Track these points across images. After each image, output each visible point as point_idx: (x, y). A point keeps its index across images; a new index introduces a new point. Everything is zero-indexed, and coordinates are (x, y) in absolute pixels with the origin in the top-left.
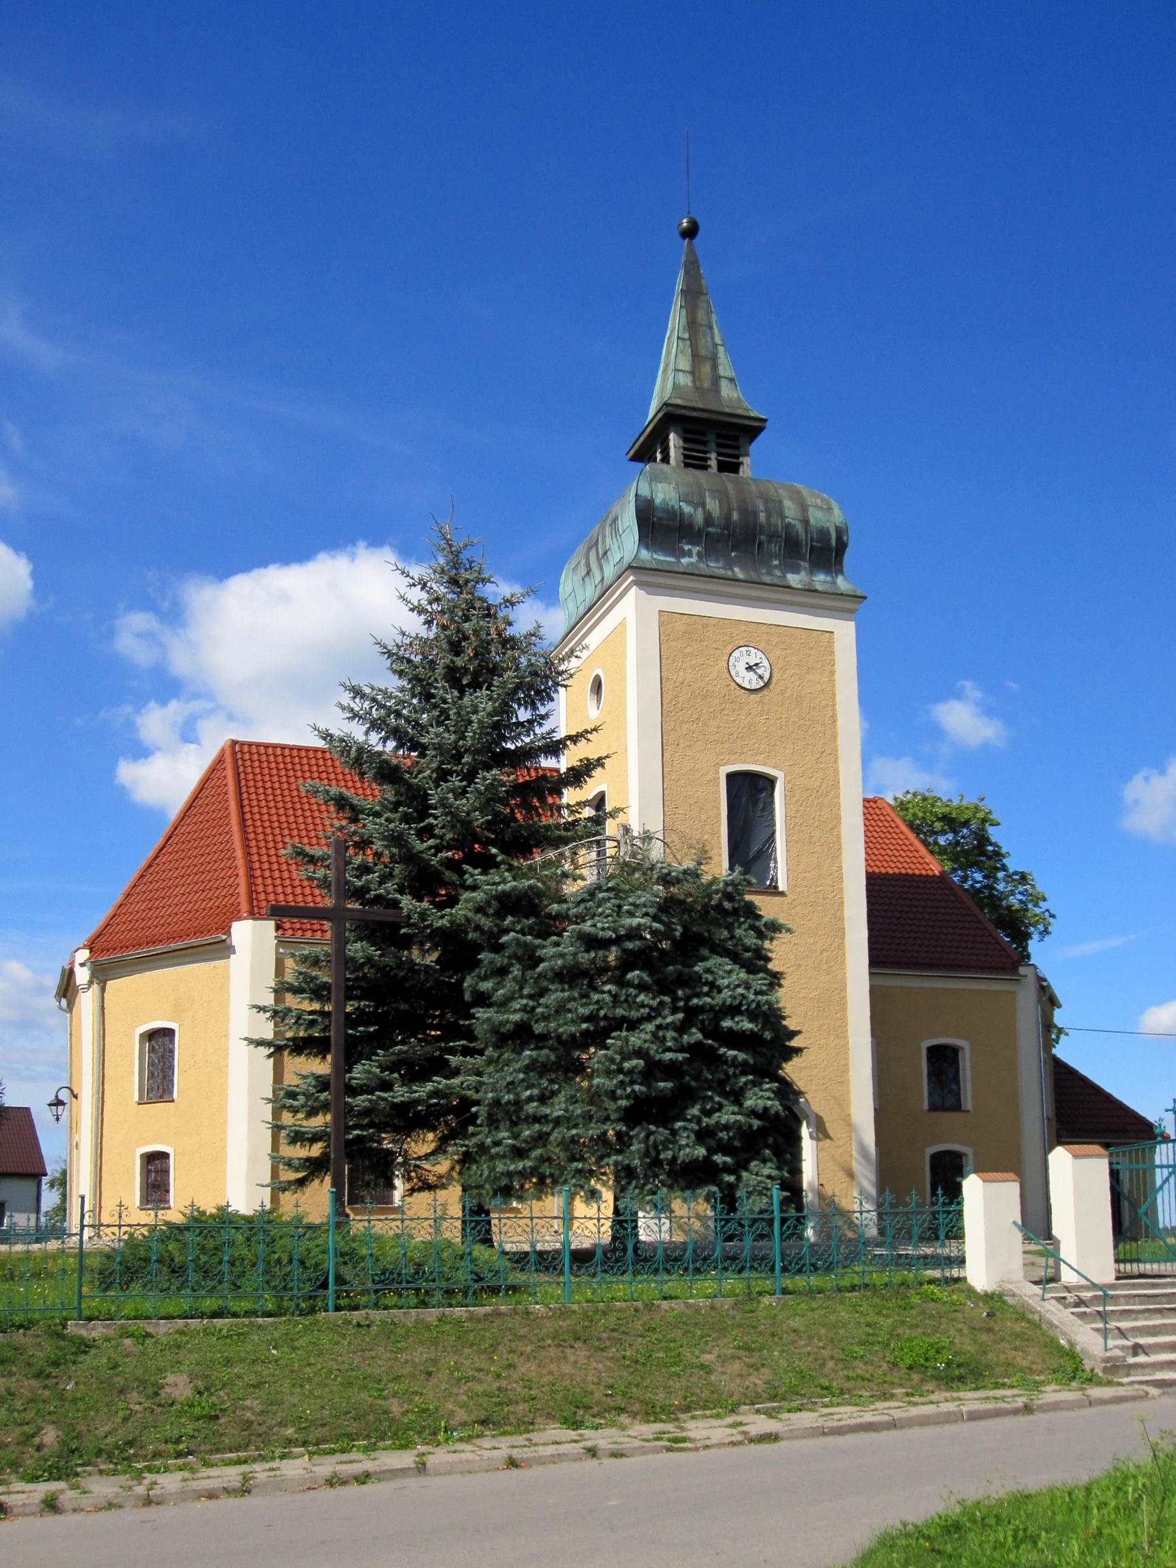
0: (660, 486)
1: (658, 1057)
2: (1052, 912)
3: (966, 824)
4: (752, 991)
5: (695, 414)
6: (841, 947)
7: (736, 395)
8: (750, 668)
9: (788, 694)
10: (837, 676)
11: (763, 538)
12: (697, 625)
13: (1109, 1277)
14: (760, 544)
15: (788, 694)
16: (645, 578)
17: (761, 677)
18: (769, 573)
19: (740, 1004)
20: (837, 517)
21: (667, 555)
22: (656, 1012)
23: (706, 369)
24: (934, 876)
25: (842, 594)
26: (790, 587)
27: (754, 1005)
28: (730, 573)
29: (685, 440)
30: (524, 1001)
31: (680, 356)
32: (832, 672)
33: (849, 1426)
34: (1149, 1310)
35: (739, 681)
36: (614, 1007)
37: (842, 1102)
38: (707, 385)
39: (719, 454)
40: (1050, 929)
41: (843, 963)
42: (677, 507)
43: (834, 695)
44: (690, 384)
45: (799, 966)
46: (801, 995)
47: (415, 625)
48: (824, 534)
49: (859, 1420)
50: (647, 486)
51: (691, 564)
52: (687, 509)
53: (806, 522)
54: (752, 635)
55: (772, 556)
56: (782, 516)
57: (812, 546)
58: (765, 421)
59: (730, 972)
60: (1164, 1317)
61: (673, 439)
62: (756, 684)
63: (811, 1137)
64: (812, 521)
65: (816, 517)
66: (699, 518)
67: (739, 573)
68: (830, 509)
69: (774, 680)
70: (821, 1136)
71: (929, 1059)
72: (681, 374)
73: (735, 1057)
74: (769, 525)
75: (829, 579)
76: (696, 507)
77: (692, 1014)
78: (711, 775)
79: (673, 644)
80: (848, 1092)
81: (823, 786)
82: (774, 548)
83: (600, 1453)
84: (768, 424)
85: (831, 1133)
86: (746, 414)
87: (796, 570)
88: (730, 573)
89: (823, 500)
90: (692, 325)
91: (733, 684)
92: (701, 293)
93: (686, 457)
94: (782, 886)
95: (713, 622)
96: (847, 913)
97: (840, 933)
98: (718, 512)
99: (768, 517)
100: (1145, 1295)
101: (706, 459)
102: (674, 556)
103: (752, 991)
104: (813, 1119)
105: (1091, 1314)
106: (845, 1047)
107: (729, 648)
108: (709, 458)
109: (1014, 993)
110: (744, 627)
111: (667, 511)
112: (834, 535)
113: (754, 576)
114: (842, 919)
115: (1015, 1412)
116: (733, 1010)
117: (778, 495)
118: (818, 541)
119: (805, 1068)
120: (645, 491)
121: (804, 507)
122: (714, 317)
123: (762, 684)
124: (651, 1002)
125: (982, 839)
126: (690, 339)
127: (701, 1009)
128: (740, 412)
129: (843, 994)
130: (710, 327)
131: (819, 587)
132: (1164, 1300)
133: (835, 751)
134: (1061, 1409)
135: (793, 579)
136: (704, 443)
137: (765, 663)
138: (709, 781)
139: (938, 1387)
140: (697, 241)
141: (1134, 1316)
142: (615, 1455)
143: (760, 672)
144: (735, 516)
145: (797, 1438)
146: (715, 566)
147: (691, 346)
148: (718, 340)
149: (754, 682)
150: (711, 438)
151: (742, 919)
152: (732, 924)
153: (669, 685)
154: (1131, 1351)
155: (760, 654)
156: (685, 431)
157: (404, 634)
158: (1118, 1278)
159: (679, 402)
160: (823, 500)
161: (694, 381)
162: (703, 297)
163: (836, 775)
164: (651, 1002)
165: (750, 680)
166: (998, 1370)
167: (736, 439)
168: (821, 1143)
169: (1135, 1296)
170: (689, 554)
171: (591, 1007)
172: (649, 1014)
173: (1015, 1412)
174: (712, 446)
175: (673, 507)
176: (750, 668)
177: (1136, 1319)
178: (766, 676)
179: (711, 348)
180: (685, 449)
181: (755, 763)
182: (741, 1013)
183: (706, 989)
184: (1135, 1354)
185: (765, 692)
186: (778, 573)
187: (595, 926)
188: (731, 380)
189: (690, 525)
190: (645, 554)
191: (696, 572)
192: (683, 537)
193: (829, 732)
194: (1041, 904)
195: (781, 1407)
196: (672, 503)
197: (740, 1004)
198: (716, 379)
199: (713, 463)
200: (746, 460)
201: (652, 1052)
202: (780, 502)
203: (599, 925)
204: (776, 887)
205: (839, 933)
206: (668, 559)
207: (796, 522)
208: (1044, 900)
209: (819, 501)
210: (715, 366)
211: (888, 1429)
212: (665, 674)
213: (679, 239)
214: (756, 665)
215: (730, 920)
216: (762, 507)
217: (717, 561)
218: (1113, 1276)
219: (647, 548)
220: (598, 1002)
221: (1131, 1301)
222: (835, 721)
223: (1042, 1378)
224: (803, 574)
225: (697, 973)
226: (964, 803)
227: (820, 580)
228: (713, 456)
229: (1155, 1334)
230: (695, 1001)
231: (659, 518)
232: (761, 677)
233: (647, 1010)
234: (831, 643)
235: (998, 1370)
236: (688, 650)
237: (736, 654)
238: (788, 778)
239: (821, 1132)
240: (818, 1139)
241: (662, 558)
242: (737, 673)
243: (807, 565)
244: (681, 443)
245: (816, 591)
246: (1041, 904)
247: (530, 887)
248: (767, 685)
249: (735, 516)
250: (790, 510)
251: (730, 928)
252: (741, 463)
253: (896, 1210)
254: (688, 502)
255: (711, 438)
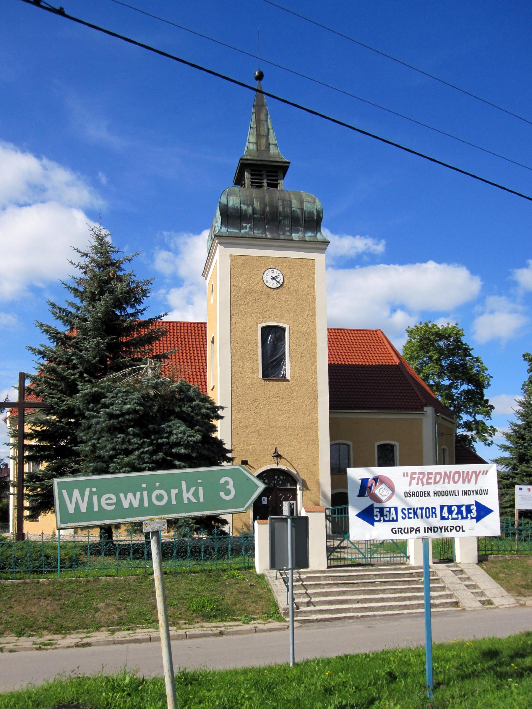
0: (231, 198)
1: (139, 466)
2: (491, 375)
3: (450, 336)
4: (186, 436)
5: (255, 162)
6: (316, 403)
7: (277, 152)
8: (273, 278)
9: (291, 289)
10: (316, 280)
11: (281, 218)
12: (248, 260)
13: (324, 567)
14: (280, 221)
15: (291, 289)
16: (222, 241)
17: (278, 282)
18: (284, 234)
19: (180, 442)
20: (318, 205)
21: (234, 229)
22: (141, 446)
23: (264, 140)
24: (396, 365)
25: (318, 241)
26: (292, 240)
27: (186, 442)
28: (264, 235)
29: (252, 175)
30: (93, 441)
31: (251, 136)
32: (314, 278)
33: (127, 640)
34: (330, 584)
35: (268, 284)
36: (123, 444)
37: (315, 473)
38: (263, 148)
39: (268, 180)
40: (490, 383)
41: (316, 412)
42: (239, 207)
43: (314, 288)
44: (255, 149)
45: (295, 413)
46: (296, 426)
47: (79, 274)
48: (311, 213)
49: (134, 638)
50: (225, 198)
51: (246, 232)
52: (244, 207)
53: (302, 209)
54: (274, 263)
55: (286, 226)
56: (291, 207)
57: (305, 220)
58: (289, 163)
59: (179, 427)
60: (338, 587)
61: (247, 175)
62: (276, 285)
63: (300, 490)
64: (305, 209)
65: (307, 207)
66: (250, 211)
67: (269, 235)
68: (315, 202)
69: (285, 283)
70: (304, 489)
71: (378, 451)
72: (251, 144)
73: (180, 464)
74: (284, 211)
75: (313, 235)
76: (248, 206)
77: (159, 448)
78: (254, 328)
79: (236, 269)
80: (318, 469)
81: (308, 331)
82: (287, 222)
83: (4, 650)
84: (291, 165)
85: (309, 486)
86: (280, 160)
87: (297, 232)
88: (264, 235)
89: (312, 198)
90: (258, 122)
91: (265, 286)
92: (263, 105)
93: (252, 182)
94: (288, 377)
95: (256, 258)
96: (319, 388)
97: (316, 397)
98: (259, 208)
99: (283, 208)
100: (334, 576)
101: (261, 183)
102: (238, 229)
103: (186, 436)
104: (301, 481)
105: (299, 586)
106: (317, 449)
107: (264, 269)
108: (263, 182)
109: (421, 419)
110: (271, 260)
111: (234, 209)
112: (315, 214)
113: (276, 236)
114: (316, 391)
115: (214, 635)
116: (177, 444)
117: (290, 197)
118: (308, 218)
119: (297, 458)
120: (224, 200)
121: (301, 202)
122: (269, 116)
123: (279, 285)
124: (139, 442)
125: (458, 340)
126: (256, 128)
127: (162, 444)
128: (278, 160)
129: (316, 425)
130: (267, 121)
131: (307, 239)
132: (345, 578)
133: (314, 315)
134: (239, 634)
135: (295, 236)
136: (261, 175)
137: (281, 275)
138: (253, 331)
139: (202, 620)
140: (262, 82)
141: (322, 587)
142: (11, 651)
143: (278, 280)
144: (268, 209)
145: (101, 645)
146: (257, 233)
147: (257, 131)
148: (270, 127)
149: (275, 285)
150: (264, 173)
151: (186, 403)
152: (181, 405)
153: (233, 289)
154: (306, 605)
155: (278, 272)
156: (252, 170)
157: (74, 278)
158: (328, 567)
159: (248, 157)
160: (312, 198)
161: (257, 147)
162: (264, 108)
163: (315, 325)
164: (139, 442)
165: (273, 284)
166: (238, 612)
167: (277, 172)
168: (304, 492)
169: (329, 577)
170: (246, 228)
171: (113, 444)
172: (138, 447)
173: (214, 635)
174: (265, 176)
175: (237, 207)
176: (273, 278)
177: (323, 588)
178: (281, 282)
179: (266, 131)
180: (251, 179)
181: (275, 321)
182: (182, 445)
183: (165, 435)
184: (308, 606)
185: (281, 289)
186: (288, 233)
187: (113, 409)
188: (276, 145)
189: (246, 215)
190: (224, 229)
191: (247, 236)
192: (243, 220)
193: (312, 305)
194: (486, 371)
195: (121, 628)
196: (237, 205)
197: (180, 442)
198: (268, 144)
199: (265, 184)
200: (281, 182)
201: (136, 464)
202: (290, 201)
203: (114, 408)
204: (285, 377)
205: (315, 396)
206: (235, 231)
207: (298, 210)
208: (487, 370)
209: (309, 199)
210: (268, 139)
211: (147, 642)
212: (232, 283)
213: (254, 80)
214: (276, 276)
215: (181, 403)
216: (280, 204)
217: (258, 230)
218: (326, 567)
219: (225, 227)
220: (116, 442)
221: (327, 579)
222: (314, 300)
223: (258, 616)
224: (300, 233)
225: (163, 428)
226: (450, 326)
227: (309, 235)
228: (265, 181)
229: (326, 596)
230: (159, 441)
231: (231, 213)
232: (278, 282)
233: (137, 445)
234: (313, 264)
235: (238, 612)
236: (244, 272)
237: (267, 272)
238: (291, 328)
239: (305, 487)
240: (303, 490)
241: (232, 231)
242: (267, 281)
243: (303, 229)
244: (250, 176)
245: (305, 241)
246: (486, 371)
247: (96, 391)
248: (282, 285)
249: (268, 209)
250: (295, 204)
251: (180, 407)
252: (279, 183)
253: (220, 537)
254: (244, 204)
255: (264, 173)
